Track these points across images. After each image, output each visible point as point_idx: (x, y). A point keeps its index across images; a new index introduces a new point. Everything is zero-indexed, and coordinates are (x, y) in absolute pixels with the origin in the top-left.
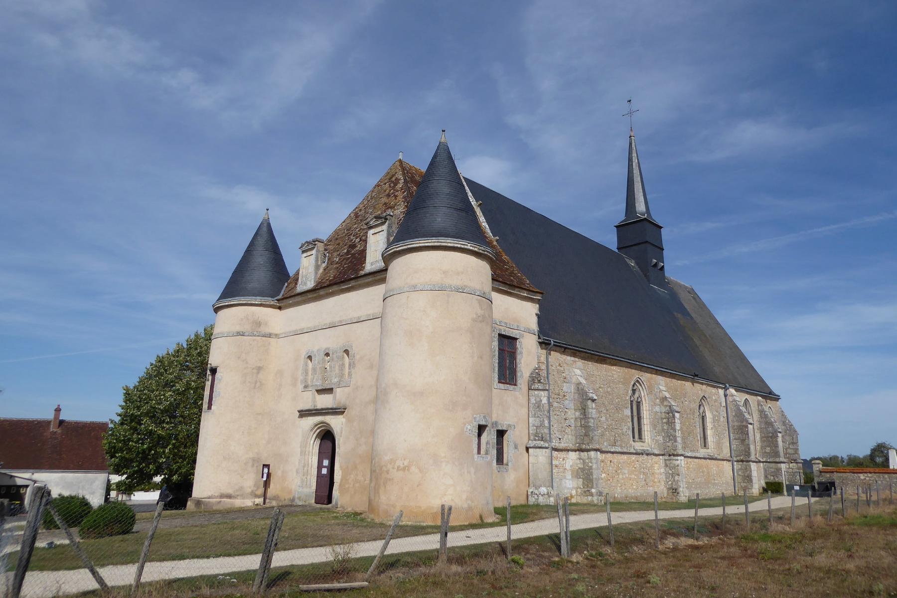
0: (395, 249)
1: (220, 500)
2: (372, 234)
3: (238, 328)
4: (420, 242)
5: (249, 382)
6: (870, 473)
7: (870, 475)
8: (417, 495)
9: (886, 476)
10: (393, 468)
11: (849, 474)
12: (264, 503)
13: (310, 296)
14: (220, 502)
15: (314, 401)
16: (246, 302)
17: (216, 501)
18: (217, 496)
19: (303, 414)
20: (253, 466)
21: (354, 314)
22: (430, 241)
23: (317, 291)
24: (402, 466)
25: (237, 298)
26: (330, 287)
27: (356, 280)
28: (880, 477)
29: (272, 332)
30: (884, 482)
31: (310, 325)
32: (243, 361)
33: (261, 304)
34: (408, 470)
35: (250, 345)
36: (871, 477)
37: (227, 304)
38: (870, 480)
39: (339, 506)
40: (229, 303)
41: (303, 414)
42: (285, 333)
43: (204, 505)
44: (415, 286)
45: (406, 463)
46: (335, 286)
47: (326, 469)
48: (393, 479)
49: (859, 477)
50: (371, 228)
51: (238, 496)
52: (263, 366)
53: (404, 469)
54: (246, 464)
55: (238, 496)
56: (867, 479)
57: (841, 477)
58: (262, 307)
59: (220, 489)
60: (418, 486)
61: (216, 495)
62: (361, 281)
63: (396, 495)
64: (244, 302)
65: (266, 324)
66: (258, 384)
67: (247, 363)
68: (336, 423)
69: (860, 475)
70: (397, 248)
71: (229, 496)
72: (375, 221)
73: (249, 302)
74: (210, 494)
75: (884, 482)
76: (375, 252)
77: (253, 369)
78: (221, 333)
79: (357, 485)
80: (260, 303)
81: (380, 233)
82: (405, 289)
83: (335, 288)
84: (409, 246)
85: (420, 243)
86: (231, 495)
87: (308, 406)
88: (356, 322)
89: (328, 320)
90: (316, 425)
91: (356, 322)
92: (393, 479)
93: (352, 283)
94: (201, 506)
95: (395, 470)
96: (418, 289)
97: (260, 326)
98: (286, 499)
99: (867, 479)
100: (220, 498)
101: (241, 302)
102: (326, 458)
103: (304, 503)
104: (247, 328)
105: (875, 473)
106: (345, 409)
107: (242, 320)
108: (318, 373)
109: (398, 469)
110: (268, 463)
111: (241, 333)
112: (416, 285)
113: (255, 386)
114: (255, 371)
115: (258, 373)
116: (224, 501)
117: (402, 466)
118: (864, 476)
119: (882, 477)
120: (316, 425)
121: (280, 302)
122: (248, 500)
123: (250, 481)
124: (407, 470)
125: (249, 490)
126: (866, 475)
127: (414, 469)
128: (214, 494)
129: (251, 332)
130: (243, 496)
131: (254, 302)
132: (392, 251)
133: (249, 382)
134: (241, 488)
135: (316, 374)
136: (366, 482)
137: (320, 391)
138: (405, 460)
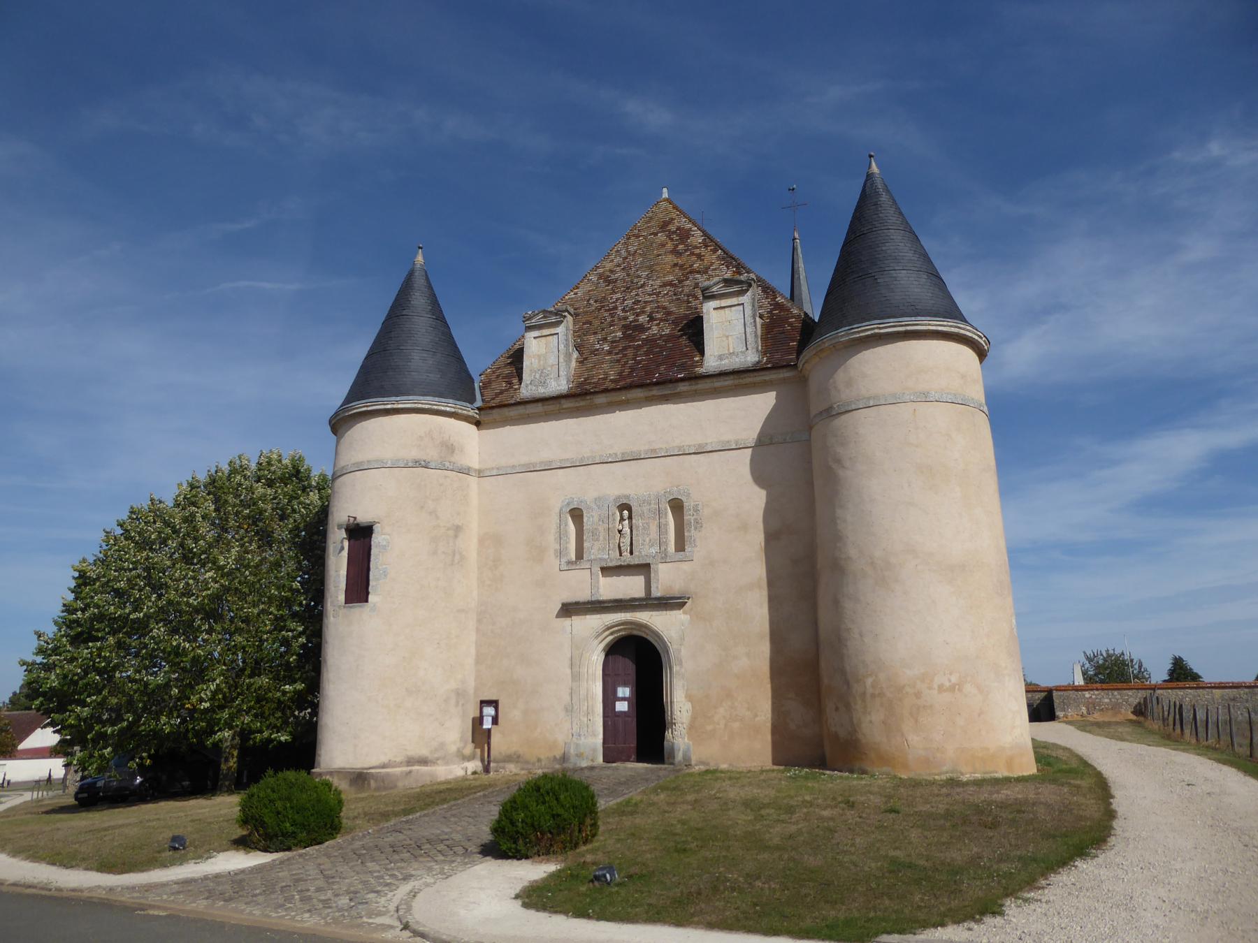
0: (877, 331)
1: (410, 768)
2: (714, 309)
3: (415, 454)
4: (930, 322)
5: (444, 552)
6: (1097, 689)
7: (1096, 692)
8: (980, 731)
9: (1116, 693)
10: (930, 688)
11: (1071, 692)
12: (487, 770)
13: (567, 404)
14: (410, 772)
15: (594, 586)
16: (430, 406)
17: (402, 772)
18: (401, 763)
19: (569, 610)
20: (457, 704)
21: (691, 440)
22: (945, 323)
23: (588, 397)
24: (947, 684)
25: (411, 397)
26: (623, 392)
27: (693, 382)
28: (1108, 694)
29: (471, 466)
30: (1113, 700)
31: (571, 454)
32: (431, 513)
33: (453, 413)
34: (960, 690)
35: (441, 485)
36: (1098, 695)
37: (389, 406)
38: (1097, 698)
39: (693, 763)
40: (395, 406)
41: (569, 610)
42: (498, 469)
43: (376, 781)
44: (926, 394)
45: (954, 679)
46: (639, 390)
47: (626, 702)
48: (931, 706)
49: (1084, 695)
50: (713, 297)
51: (438, 759)
52: (463, 524)
53: (952, 689)
54: (446, 701)
55: (438, 759)
56: (1093, 697)
57: (1061, 696)
58: (453, 419)
59: (406, 750)
60: (979, 715)
61: (398, 760)
62: (702, 385)
63: (942, 732)
64: (427, 406)
65: (462, 451)
66: (457, 557)
67: (437, 518)
68: (660, 622)
69: (1084, 693)
70: (880, 328)
71: (424, 761)
72: (722, 287)
73: (435, 407)
74: (384, 759)
75: (1113, 700)
76: (725, 339)
77: (448, 529)
78: (377, 461)
79: (736, 725)
80: (453, 410)
81: (733, 308)
82: (907, 398)
83: (638, 393)
84: (909, 328)
85: (929, 325)
86: (427, 758)
87: (584, 595)
88: (694, 453)
89: (619, 449)
90: (608, 628)
91: (694, 453)
92: (931, 706)
93: (683, 387)
94: (369, 784)
95: (935, 692)
96: (931, 399)
97: (453, 452)
98: (542, 757)
99: (1093, 697)
100: (408, 766)
101: (420, 406)
102: (625, 685)
103: (590, 764)
104: (432, 454)
105: (1103, 689)
106: (688, 598)
107: (421, 438)
108: (601, 538)
109: (941, 689)
110: (494, 698)
111: (423, 463)
112: (928, 393)
113: (453, 561)
114: (451, 533)
115: (456, 537)
116: (418, 770)
117: (947, 684)
118: (1089, 693)
119: (1110, 694)
120: (608, 628)
121: (482, 412)
122: (455, 766)
123: (455, 733)
124: (958, 690)
125: (453, 749)
126: (1092, 692)
127: (968, 688)
128: (393, 759)
129: (439, 461)
130: (446, 760)
131: (443, 408)
132: (869, 333)
133: (444, 552)
134: (442, 745)
135: (598, 540)
136: (757, 719)
137: (607, 571)
138: (951, 674)
